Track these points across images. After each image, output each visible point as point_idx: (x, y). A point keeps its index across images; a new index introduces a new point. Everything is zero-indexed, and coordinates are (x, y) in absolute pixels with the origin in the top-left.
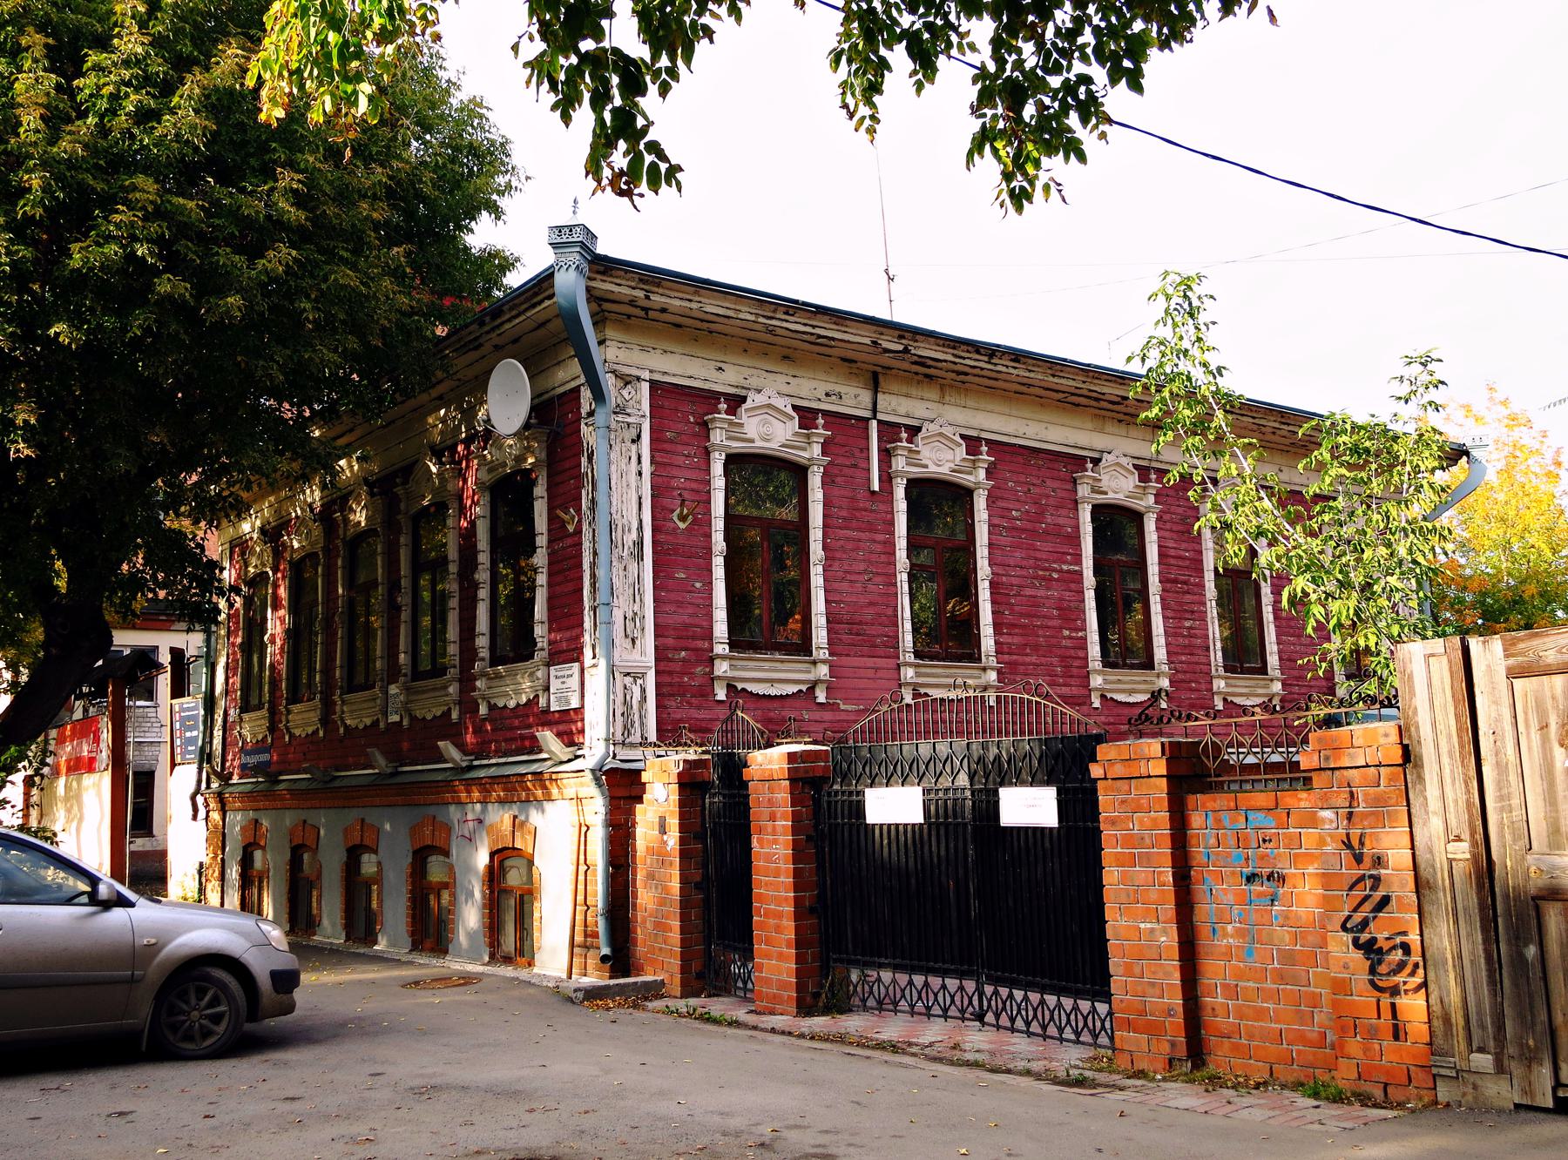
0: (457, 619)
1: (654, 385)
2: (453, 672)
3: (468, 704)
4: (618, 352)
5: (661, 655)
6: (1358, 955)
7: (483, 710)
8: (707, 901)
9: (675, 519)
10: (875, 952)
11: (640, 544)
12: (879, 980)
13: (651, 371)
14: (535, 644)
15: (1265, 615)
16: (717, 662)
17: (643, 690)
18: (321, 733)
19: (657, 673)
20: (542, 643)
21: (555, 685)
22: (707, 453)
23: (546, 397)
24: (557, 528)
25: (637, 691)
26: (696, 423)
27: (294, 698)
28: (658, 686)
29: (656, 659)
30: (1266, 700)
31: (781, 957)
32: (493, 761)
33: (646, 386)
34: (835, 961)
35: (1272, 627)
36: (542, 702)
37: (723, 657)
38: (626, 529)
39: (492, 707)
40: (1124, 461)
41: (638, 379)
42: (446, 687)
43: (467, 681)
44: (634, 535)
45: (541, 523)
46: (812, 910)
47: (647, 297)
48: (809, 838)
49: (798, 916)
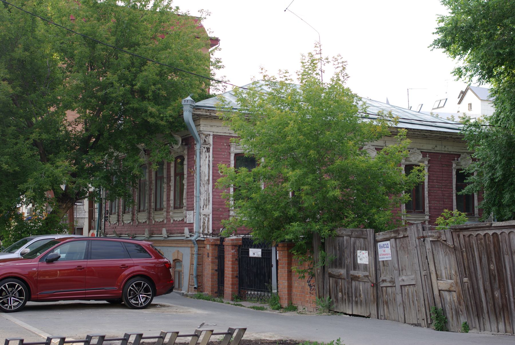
0: (166, 195)
1: (214, 136)
2: (164, 210)
3: (169, 220)
4: (203, 127)
5: (214, 210)
6: (309, 287)
7: (172, 221)
8: (218, 274)
9: (219, 173)
10: (251, 287)
11: (209, 180)
12: (248, 293)
13: (213, 132)
14: (183, 205)
15: (425, 194)
16: (230, 211)
17: (209, 219)
18: (132, 223)
19: (212, 214)
20: (185, 204)
21: (188, 216)
22: (230, 154)
23: (187, 136)
24: (189, 173)
25: (207, 219)
26: (226, 146)
27: (124, 212)
28: (213, 218)
29: (213, 211)
30: (423, 222)
31: (229, 288)
32: (66, 272)
33: (211, 137)
34: (242, 289)
35: (427, 198)
36: (185, 220)
37: (232, 210)
38: (205, 176)
39: (174, 220)
40: (372, 147)
41: (209, 135)
42: (163, 214)
43: (168, 212)
44: (207, 178)
45: (185, 172)
46: (236, 277)
47: (210, 114)
48: (236, 260)
49: (232, 278)
